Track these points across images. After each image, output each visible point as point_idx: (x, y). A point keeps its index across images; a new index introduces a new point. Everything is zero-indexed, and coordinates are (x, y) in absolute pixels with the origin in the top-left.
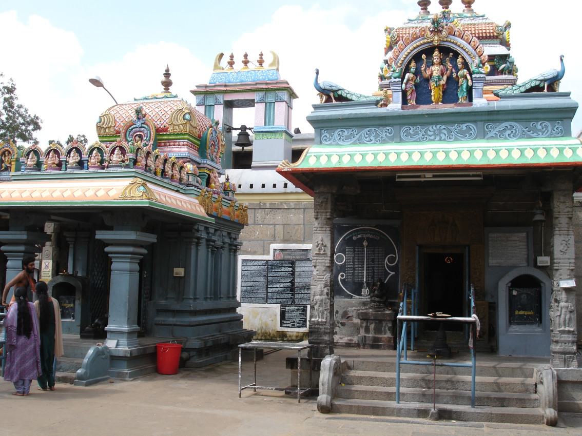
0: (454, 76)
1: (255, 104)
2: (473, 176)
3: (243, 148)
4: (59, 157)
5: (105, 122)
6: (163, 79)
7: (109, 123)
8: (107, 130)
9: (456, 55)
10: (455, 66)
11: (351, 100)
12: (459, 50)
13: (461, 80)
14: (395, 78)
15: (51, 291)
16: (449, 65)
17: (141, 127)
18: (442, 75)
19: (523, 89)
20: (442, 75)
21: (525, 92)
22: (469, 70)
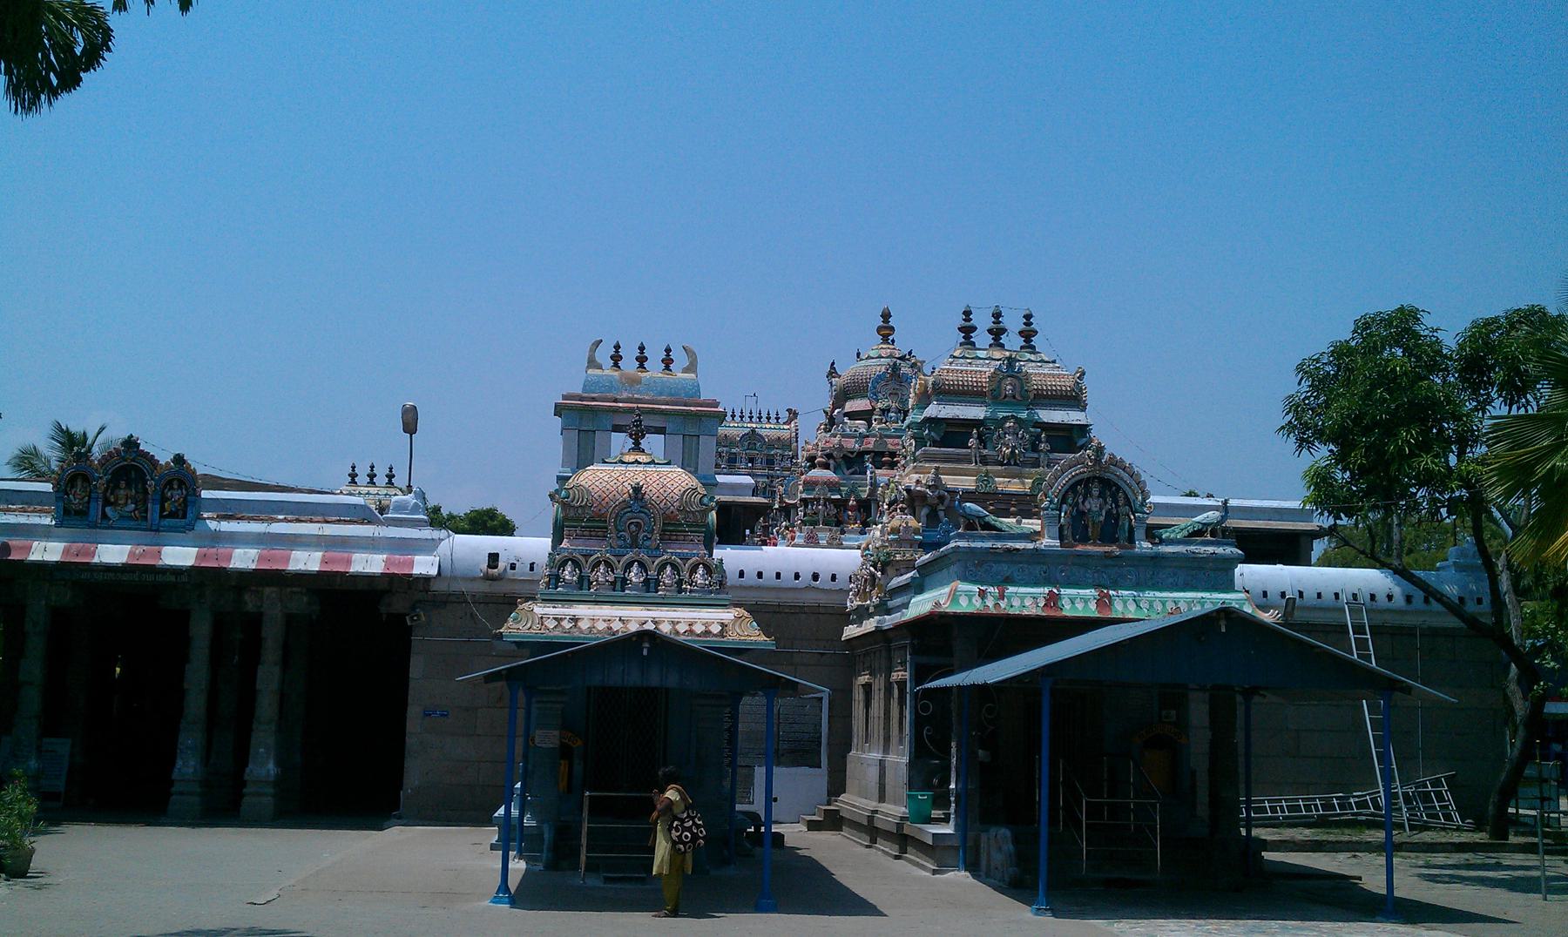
0: (690, 811)
1: (1396, 894)
2: (1441, 867)
3: (1052, 600)
4: (646, 572)
5: (577, 497)
6: (637, 352)
7: (583, 500)
8: (580, 511)
9: (1119, 488)
10: (1115, 501)
11: (1000, 530)
12: (1120, 483)
13: (1122, 517)
14: (1052, 510)
15: (964, 606)
16: (1109, 500)
17: (640, 512)
18: (1101, 509)
19: (1186, 533)
20: (1101, 509)
21: (1188, 536)
22: (1131, 507)
